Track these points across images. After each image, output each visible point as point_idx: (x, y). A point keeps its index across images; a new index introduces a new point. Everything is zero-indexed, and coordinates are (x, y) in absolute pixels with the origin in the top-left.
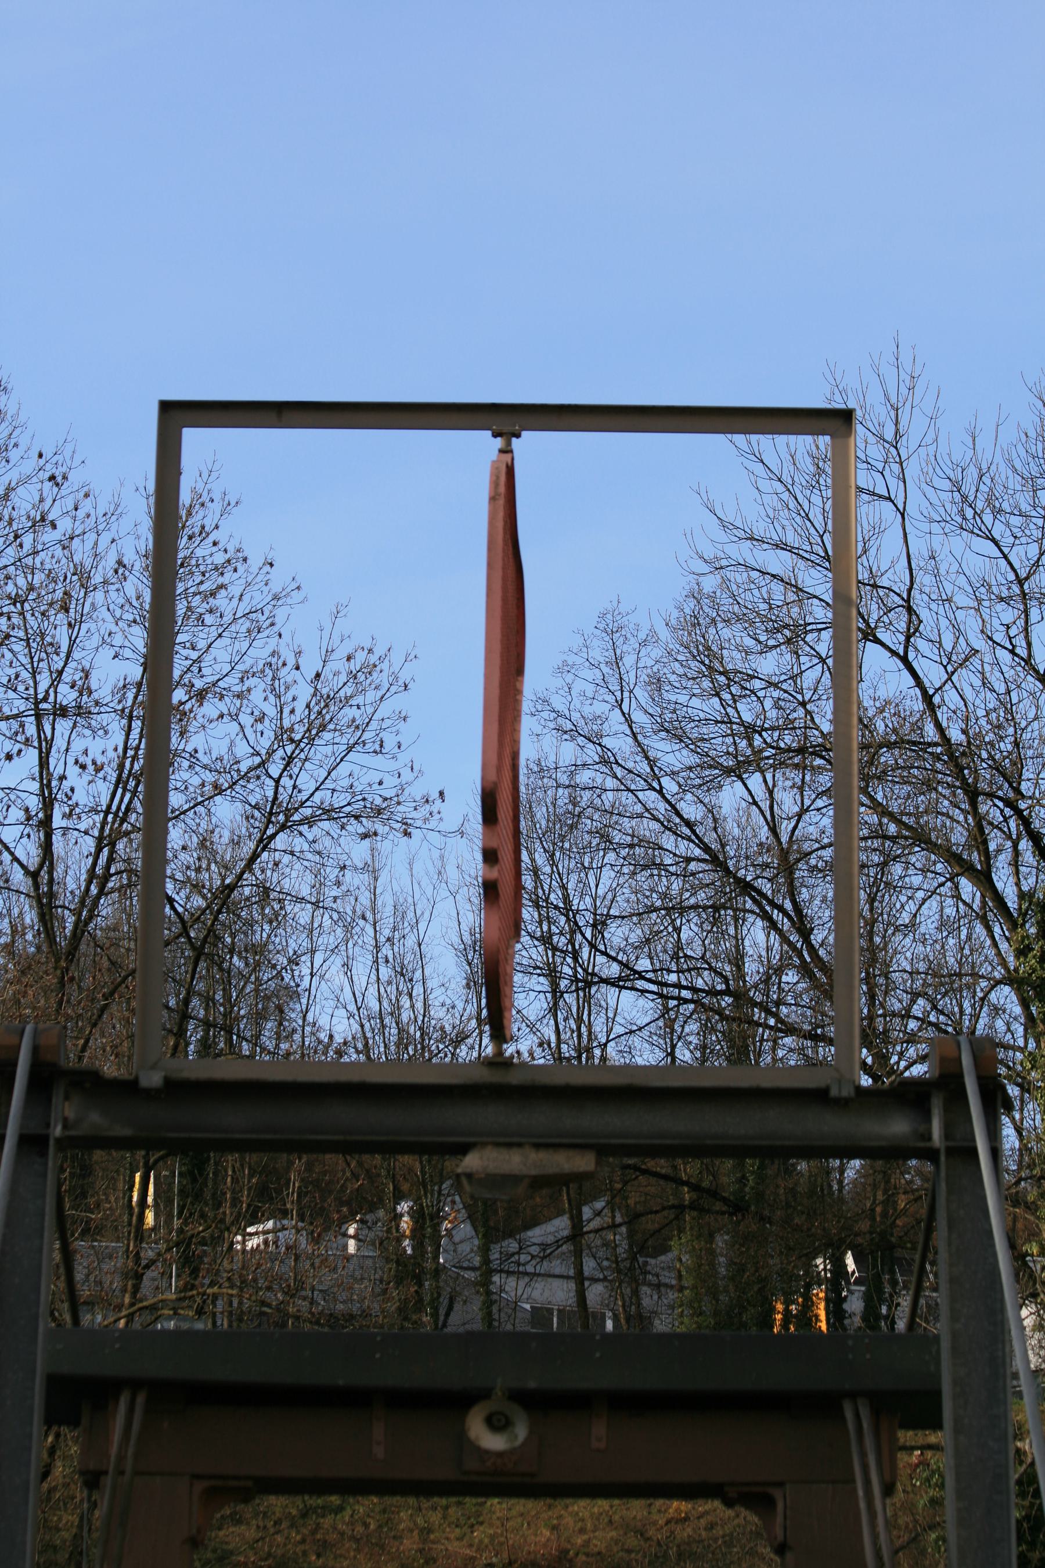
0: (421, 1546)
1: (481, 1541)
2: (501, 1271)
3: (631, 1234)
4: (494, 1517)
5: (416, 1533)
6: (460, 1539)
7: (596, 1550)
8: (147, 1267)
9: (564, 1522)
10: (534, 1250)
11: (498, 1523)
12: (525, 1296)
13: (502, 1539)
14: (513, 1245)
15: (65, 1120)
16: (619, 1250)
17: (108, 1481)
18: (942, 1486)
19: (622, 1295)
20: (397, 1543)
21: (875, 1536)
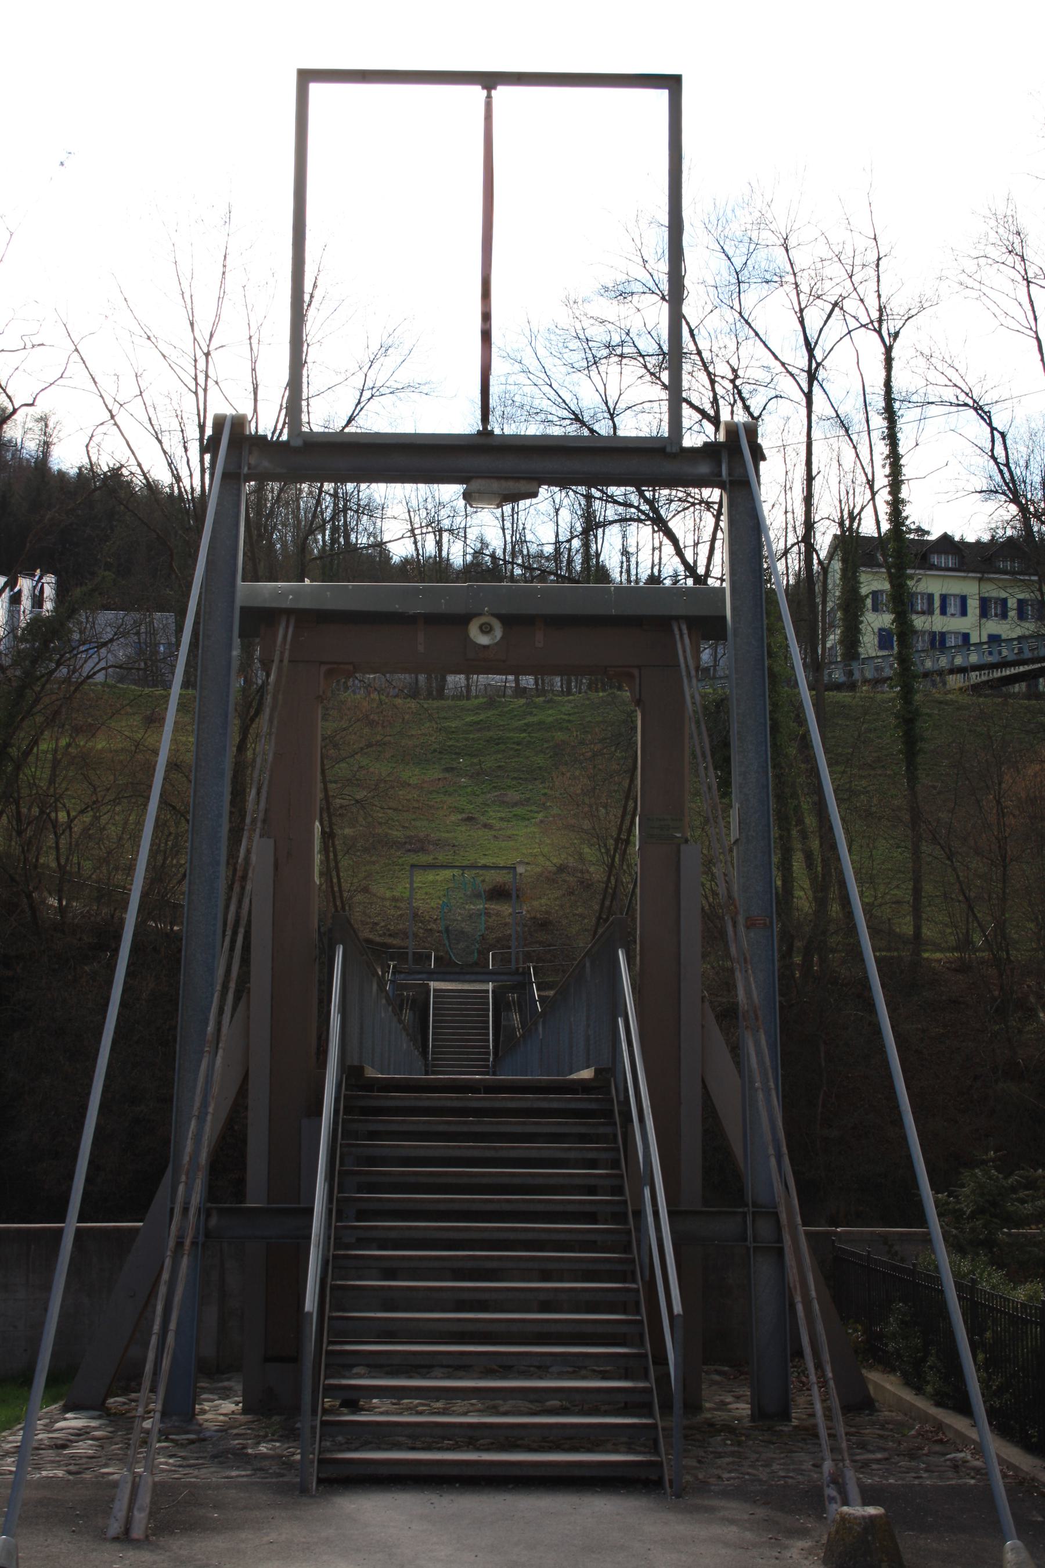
15: (249, 464)
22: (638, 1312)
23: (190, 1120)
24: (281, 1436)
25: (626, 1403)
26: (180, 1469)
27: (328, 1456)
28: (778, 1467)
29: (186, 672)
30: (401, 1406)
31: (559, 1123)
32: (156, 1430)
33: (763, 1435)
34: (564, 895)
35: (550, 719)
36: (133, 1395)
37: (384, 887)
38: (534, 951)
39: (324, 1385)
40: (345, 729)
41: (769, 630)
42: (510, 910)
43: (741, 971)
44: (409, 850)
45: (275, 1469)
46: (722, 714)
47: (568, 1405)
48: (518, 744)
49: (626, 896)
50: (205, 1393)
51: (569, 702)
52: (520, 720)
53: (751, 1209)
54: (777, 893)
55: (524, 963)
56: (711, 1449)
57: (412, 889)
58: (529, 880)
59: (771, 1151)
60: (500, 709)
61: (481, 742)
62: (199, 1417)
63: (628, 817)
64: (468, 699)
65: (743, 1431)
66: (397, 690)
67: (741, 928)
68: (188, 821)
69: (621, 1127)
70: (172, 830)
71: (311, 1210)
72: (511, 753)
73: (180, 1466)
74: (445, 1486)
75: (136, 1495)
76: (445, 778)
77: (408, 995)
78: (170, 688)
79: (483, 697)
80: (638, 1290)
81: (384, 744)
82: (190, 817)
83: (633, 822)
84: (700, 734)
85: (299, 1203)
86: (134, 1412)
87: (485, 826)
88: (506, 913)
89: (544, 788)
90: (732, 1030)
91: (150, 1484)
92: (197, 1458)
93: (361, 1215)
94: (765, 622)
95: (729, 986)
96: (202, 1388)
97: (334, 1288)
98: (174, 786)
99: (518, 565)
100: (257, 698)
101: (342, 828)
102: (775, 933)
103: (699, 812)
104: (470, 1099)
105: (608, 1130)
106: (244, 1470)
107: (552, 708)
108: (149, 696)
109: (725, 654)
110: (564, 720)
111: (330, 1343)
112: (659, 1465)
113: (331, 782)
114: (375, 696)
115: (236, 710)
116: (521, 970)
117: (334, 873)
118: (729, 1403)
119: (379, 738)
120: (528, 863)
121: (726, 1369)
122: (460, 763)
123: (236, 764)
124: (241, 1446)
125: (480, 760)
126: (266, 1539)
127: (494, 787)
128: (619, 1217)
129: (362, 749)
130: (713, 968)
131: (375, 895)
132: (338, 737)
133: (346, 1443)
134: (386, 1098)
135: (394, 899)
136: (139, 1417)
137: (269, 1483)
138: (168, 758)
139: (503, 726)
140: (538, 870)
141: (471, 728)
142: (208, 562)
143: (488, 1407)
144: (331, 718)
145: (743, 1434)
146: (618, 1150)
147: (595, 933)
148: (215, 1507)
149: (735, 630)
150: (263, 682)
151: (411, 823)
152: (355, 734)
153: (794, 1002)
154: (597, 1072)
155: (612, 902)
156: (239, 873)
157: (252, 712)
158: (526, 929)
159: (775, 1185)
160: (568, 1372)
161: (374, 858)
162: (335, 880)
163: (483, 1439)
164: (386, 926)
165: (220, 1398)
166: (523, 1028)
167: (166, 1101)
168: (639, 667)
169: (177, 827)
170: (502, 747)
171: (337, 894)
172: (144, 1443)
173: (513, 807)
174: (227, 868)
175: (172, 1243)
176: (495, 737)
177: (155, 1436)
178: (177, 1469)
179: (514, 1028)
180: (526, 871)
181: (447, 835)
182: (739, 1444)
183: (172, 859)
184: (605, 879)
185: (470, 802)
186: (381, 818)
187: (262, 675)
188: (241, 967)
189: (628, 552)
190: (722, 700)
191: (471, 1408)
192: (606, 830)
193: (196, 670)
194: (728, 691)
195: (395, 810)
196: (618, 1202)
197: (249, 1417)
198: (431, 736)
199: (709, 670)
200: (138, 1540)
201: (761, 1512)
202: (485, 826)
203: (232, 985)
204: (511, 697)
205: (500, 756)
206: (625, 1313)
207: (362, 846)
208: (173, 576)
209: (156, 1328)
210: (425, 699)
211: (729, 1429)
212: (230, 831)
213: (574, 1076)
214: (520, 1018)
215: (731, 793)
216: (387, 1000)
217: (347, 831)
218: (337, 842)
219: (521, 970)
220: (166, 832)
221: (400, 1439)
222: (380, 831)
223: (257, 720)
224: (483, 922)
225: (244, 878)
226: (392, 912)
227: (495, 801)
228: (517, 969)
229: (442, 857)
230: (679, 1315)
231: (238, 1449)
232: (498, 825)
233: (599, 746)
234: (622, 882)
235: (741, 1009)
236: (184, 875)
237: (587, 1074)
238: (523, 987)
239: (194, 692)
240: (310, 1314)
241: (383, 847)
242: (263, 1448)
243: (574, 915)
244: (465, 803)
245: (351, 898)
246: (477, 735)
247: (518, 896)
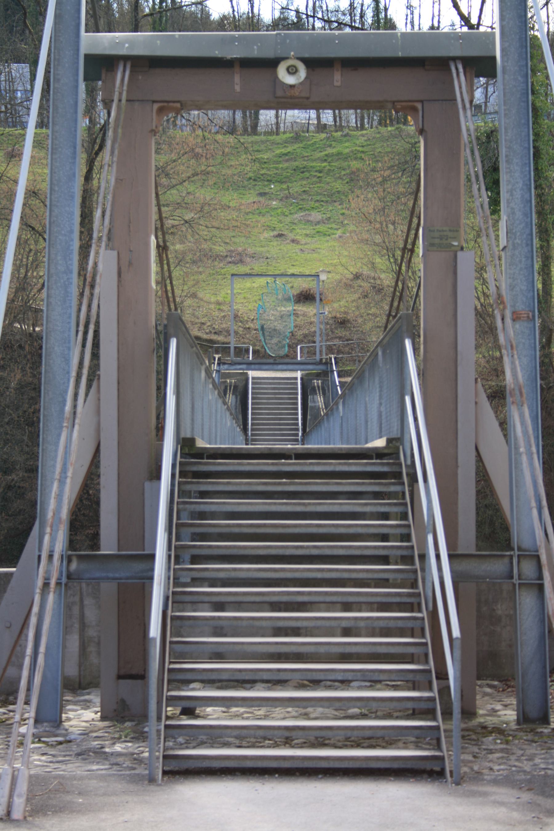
22: (423, 636)
23: (52, 483)
24: (132, 738)
25: (414, 710)
26: (51, 764)
27: (171, 752)
28: (540, 761)
29: (40, 114)
30: (230, 714)
31: (357, 484)
32: (30, 734)
33: (527, 735)
34: (360, 298)
35: (347, 151)
36: (11, 707)
37: (210, 293)
38: (335, 345)
39: (167, 696)
40: (174, 161)
41: (532, 70)
42: (315, 311)
43: (508, 355)
44: (230, 262)
45: (128, 763)
46: (492, 143)
47: (366, 712)
48: (320, 172)
49: (411, 298)
50: (69, 704)
51: (363, 135)
52: (321, 152)
53: (517, 553)
54: (538, 294)
55: (327, 354)
56: (484, 747)
57: (233, 294)
58: (331, 286)
59: (533, 504)
60: (304, 143)
61: (289, 171)
62: (65, 724)
63: (413, 232)
64: (277, 134)
65: (511, 733)
66: (217, 127)
67: (508, 320)
68: (44, 239)
69: (409, 486)
70: (32, 247)
71: (152, 557)
72: (315, 179)
73: (51, 762)
74: (266, 776)
75: (15, 785)
76: (259, 202)
77: (231, 383)
78: (27, 128)
79: (290, 133)
80: (423, 619)
81: (208, 173)
82: (46, 236)
83: (416, 235)
84: (474, 160)
85: (144, 550)
86: (12, 720)
87: (293, 241)
88: (312, 313)
89: (343, 209)
90: (500, 408)
91: (27, 775)
92: (65, 756)
93: (195, 559)
94: (529, 63)
95: (498, 372)
96: (68, 701)
97: (173, 618)
98: (33, 210)
99: (319, 19)
100: (100, 136)
101: (173, 244)
102: (537, 328)
103: (472, 227)
104: (284, 464)
105: (398, 488)
106: (103, 765)
107: (348, 141)
108: (10, 135)
109: (494, 92)
110: (359, 151)
111: (170, 663)
112: (442, 759)
113: (164, 206)
114: (199, 132)
115: (83, 146)
116: (324, 361)
117: (168, 281)
118: (498, 711)
119: (203, 168)
120: (329, 272)
121: (496, 683)
122: (271, 188)
123: (84, 191)
124: (99, 746)
125: (288, 186)
126: (121, 819)
127: (300, 209)
128: (408, 559)
129: (189, 177)
130: (484, 357)
131: (202, 300)
132: (169, 167)
133: (186, 743)
134: (214, 464)
135: (218, 303)
136: (17, 722)
137: (124, 775)
138: (27, 186)
139: (307, 156)
140: (338, 277)
141: (280, 159)
142: (56, 16)
143: (301, 714)
144: (162, 152)
145: (511, 735)
146: (406, 504)
147: (386, 327)
148: (80, 794)
149: (504, 68)
150: (105, 122)
151: (231, 240)
152: (183, 164)
153: (551, 385)
154: (389, 441)
155: (399, 302)
156: (89, 279)
157: (97, 147)
158: (328, 326)
159: (537, 532)
160: (366, 686)
161: (201, 269)
162: (169, 288)
163: (297, 739)
164: (212, 325)
165: (82, 709)
166: (326, 408)
167: (33, 470)
168: (422, 101)
169: (36, 245)
170: (307, 174)
171: (171, 299)
172: (21, 744)
173: (316, 225)
174: (79, 278)
175: (40, 583)
176: (301, 166)
177: (29, 738)
178: (48, 764)
179: (319, 408)
180: (328, 278)
181: (262, 249)
182: (507, 742)
183: (33, 272)
184: (394, 284)
185: (280, 222)
186: (206, 235)
187: (104, 115)
188: (92, 360)
189: (411, 6)
190: (492, 132)
191: (287, 715)
192: (394, 242)
193: (48, 112)
194: (497, 123)
195: (218, 228)
196: (407, 547)
197: (106, 723)
198: (247, 166)
199: (481, 106)
200: (17, 821)
201: (526, 797)
202: (293, 241)
203: (85, 371)
204: (313, 132)
205: (305, 182)
206: (412, 636)
207: (191, 259)
208: (27, 32)
209: (29, 651)
210: (241, 135)
211: (499, 731)
212: (81, 247)
213: (370, 445)
214: (324, 400)
215: (500, 210)
216: (213, 386)
217: (178, 247)
218: (170, 256)
219: (324, 361)
220: (27, 249)
221: (230, 740)
222: (206, 246)
223: (101, 154)
224: (292, 321)
225: (92, 287)
226: (217, 313)
227: (301, 220)
228: (321, 360)
229: (257, 267)
230: (457, 638)
231: (98, 748)
232: (303, 240)
233: (387, 173)
234: (408, 287)
235: (508, 388)
236: (43, 285)
237: (380, 443)
238: (325, 374)
239: (47, 131)
240: (154, 639)
241: (208, 259)
242: (118, 748)
243: (368, 314)
244: (276, 223)
245: (182, 302)
246: (286, 165)
247: (321, 300)
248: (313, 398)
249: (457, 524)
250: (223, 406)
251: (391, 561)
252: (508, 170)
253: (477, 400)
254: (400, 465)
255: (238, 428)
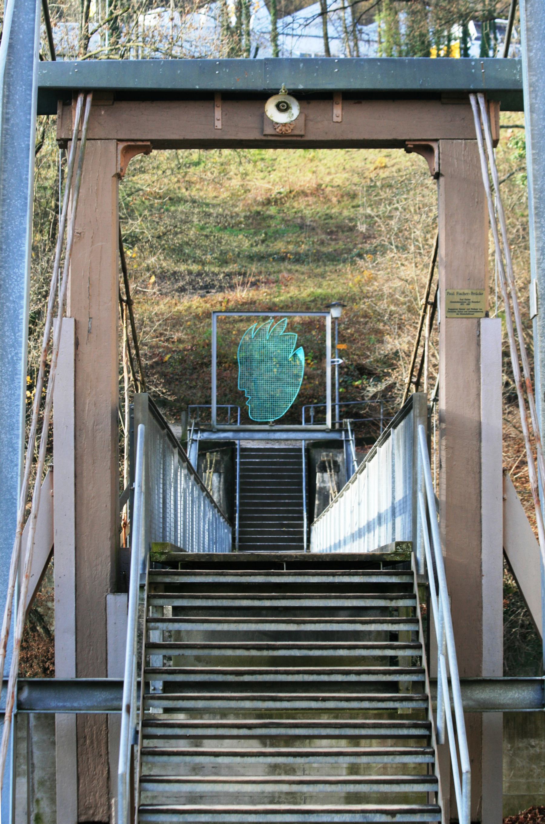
0: (242, 183)
1: (274, 180)
2: (283, 34)
3: (353, 13)
4: (282, 166)
5: (239, 176)
6: (263, 179)
7: (337, 184)
8: (92, 34)
9: (319, 169)
10: (302, 21)
11: (284, 170)
12: (296, 47)
13: (286, 179)
14: (289, 19)
16: (347, 22)
17: (71, 144)
18: (524, 148)
19: (349, 46)
20: (229, 182)
21: (488, 170)
85: (107, 677)
248: (323, 477)
249: (481, 644)
250: (201, 492)
251: (401, 688)
252: (538, 225)
253: (505, 496)
254: (412, 574)
255: (221, 518)
